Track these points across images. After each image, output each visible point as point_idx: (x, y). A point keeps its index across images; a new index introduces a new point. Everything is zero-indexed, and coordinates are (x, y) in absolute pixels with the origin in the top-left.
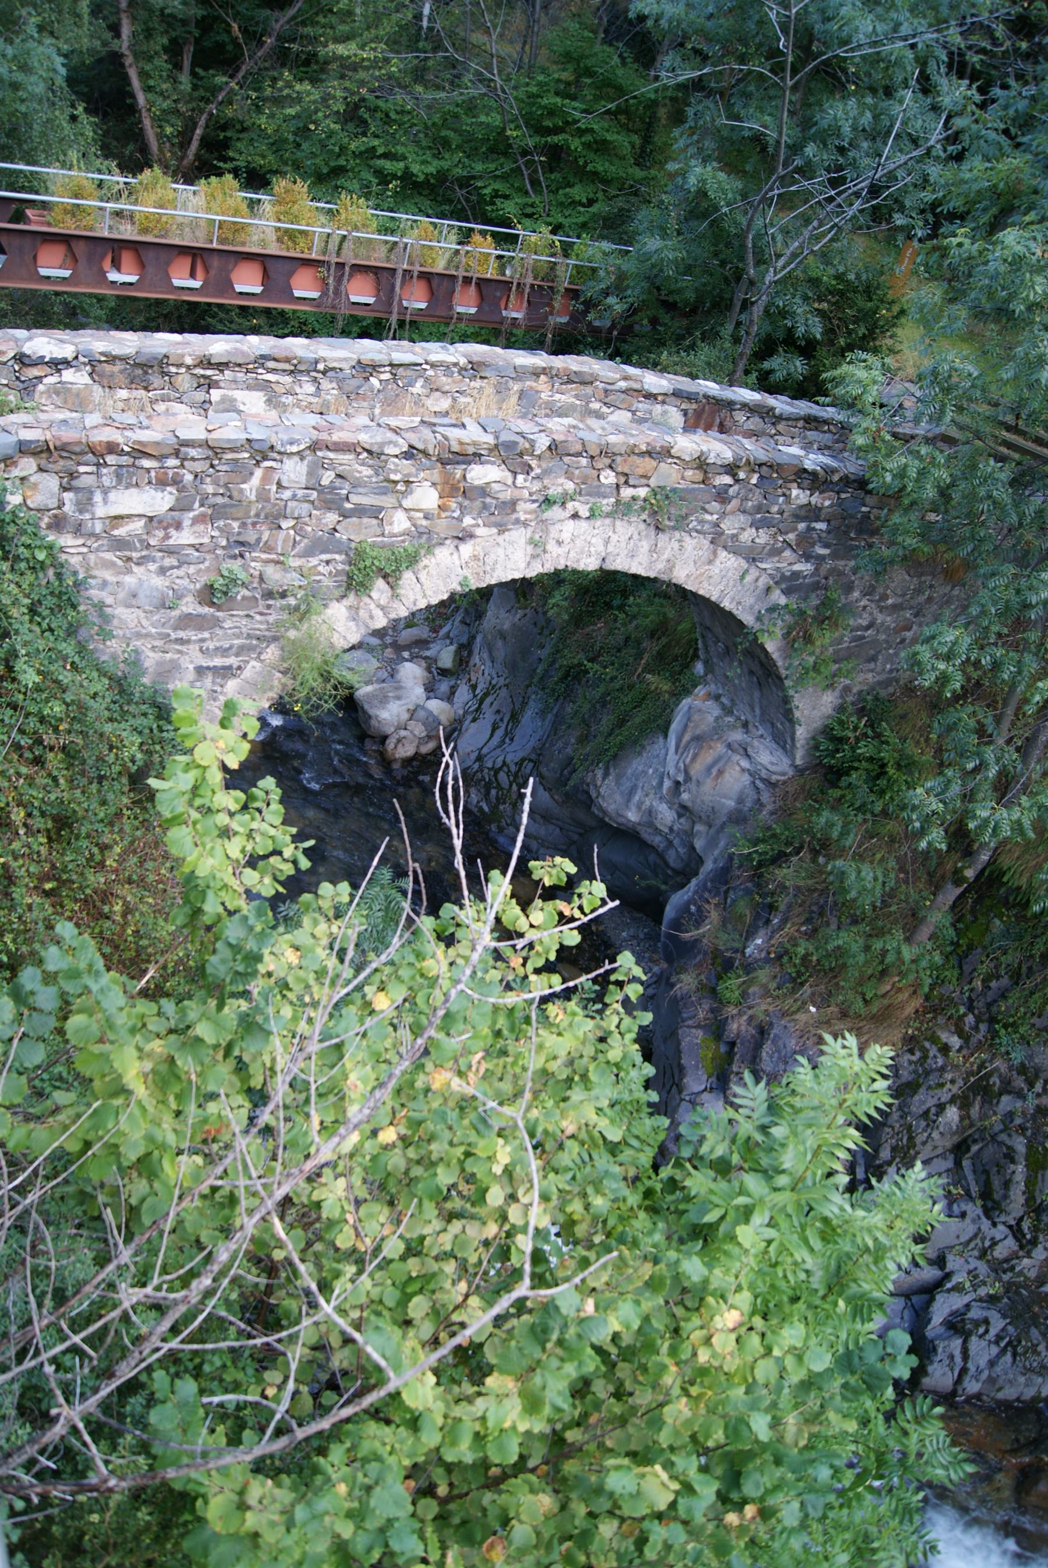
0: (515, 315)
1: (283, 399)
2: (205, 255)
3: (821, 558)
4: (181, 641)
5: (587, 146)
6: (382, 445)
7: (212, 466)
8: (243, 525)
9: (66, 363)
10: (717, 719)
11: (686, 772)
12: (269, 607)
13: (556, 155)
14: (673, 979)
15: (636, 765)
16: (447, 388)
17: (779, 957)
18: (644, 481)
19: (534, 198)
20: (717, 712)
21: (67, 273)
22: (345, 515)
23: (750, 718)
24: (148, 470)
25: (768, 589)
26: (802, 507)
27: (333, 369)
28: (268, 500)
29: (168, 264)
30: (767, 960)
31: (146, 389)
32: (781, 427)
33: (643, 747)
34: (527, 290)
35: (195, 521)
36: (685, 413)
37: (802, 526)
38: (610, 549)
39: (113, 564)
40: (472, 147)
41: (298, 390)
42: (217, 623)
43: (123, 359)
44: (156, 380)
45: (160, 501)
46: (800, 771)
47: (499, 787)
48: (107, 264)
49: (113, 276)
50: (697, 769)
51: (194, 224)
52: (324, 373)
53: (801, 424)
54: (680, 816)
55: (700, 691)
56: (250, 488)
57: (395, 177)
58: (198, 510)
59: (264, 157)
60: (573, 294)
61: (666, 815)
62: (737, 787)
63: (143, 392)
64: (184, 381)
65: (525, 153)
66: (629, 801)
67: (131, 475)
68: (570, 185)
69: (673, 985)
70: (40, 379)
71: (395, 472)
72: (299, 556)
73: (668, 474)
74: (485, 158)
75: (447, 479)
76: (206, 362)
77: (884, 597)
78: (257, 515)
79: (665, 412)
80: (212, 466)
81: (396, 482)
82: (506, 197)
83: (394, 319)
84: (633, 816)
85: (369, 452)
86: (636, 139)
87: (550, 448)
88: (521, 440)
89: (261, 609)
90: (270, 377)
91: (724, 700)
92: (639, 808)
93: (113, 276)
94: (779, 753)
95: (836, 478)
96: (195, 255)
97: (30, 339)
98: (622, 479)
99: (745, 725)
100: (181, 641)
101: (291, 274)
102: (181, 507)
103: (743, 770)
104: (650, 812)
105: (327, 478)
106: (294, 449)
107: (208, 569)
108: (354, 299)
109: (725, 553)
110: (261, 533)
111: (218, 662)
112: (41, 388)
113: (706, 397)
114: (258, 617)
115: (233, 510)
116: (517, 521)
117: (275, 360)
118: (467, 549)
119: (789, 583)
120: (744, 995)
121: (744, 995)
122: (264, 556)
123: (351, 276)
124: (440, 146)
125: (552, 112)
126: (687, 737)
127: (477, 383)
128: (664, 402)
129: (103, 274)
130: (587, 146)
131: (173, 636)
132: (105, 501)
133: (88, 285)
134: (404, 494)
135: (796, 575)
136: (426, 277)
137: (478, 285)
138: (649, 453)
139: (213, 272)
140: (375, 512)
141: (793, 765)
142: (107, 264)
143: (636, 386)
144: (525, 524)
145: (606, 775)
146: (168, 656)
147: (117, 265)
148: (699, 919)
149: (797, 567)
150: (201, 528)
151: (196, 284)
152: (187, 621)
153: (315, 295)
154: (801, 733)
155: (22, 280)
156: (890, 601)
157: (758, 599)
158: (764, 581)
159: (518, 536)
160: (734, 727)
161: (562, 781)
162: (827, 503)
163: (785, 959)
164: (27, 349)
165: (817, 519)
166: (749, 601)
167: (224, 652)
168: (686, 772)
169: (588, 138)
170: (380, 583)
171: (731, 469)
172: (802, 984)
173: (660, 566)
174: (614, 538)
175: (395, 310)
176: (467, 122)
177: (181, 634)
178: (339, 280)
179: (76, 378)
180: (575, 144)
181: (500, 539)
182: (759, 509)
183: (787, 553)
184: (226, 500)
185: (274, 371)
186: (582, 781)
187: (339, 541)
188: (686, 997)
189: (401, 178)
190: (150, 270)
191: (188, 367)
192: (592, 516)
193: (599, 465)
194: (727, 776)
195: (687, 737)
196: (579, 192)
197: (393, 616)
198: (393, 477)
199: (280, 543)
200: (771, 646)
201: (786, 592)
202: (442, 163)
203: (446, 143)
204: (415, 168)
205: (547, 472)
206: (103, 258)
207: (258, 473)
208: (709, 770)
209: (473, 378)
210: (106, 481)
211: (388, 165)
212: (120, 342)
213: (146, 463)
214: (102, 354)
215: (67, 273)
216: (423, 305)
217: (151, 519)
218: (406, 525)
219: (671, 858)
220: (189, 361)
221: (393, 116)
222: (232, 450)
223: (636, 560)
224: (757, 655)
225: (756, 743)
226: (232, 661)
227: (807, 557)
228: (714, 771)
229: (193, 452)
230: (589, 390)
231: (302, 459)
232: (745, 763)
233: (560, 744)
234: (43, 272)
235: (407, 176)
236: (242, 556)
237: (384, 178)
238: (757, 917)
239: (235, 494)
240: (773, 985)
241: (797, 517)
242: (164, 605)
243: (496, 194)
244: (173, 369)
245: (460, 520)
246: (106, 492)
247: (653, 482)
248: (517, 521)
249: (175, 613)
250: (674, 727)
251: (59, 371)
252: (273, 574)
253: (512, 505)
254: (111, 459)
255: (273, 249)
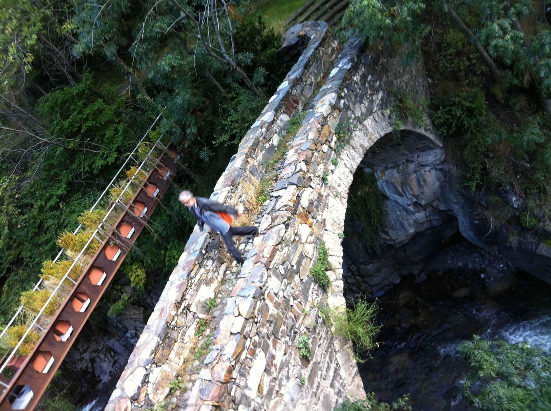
0: (168, 175)
1: (209, 277)
2: (78, 291)
3: (380, 85)
4: (318, 387)
5: (93, 119)
6: (279, 235)
7: (256, 323)
8: (284, 323)
9: (147, 376)
10: (398, 172)
11: (414, 196)
12: (319, 333)
13: (91, 133)
14: (508, 245)
15: (391, 218)
16: (236, 202)
17: (526, 193)
18: (331, 135)
19: (101, 152)
20: (395, 171)
21: (52, 360)
22: (297, 272)
23: (406, 158)
24: (247, 358)
25: (383, 114)
26: (361, 80)
27: (207, 246)
28: (280, 304)
29: (73, 309)
30: (524, 199)
31: (176, 341)
32: (304, 79)
33: (386, 211)
34: (161, 164)
35: (275, 347)
36: (284, 112)
37: (367, 85)
38: (348, 166)
39: (276, 403)
40: (63, 166)
41: (208, 268)
42: (317, 363)
43: (158, 345)
44: (174, 334)
45: (261, 360)
46: (445, 147)
47: (353, 285)
48: (58, 338)
49: (64, 338)
50: (416, 190)
51: (62, 289)
52: (207, 252)
53: (306, 71)
54: (425, 210)
55: (378, 175)
56: (273, 310)
57: (58, 203)
58: (270, 342)
59: (10, 255)
60: (172, 148)
61: (420, 216)
62: (434, 177)
63: (176, 344)
64: (181, 320)
65: (81, 145)
66: (405, 229)
67: (244, 368)
68: (104, 135)
69: (511, 247)
70: (147, 395)
71: (291, 237)
72: (305, 304)
73: (333, 123)
74: (72, 162)
75: (300, 215)
76: (178, 304)
77: (399, 72)
78: (283, 314)
79: (281, 121)
80: (256, 323)
81: (294, 240)
82: (93, 163)
83: (145, 223)
84: (412, 231)
85: (280, 243)
86: (100, 100)
87: (306, 164)
88: (299, 174)
89: (318, 338)
90: (198, 277)
91: (389, 166)
92: (410, 225)
93: (64, 338)
94: (431, 152)
95: (356, 59)
96: (77, 295)
97: (123, 390)
98: (328, 143)
99: (408, 161)
100: (318, 387)
101: (105, 257)
102: (265, 349)
103: (429, 171)
104: (415, 222)
105: (282, 270)
106: (265, 277)
107: (295, 354)
108: (129, 236)
109: (365, 122)
110: (291, 317)
111: (331, 373)
112: (151, 397)
113: (282, 100)
114: (321, 341)
115: (278, 324)
116: (326, 197)
117: (192, 271)
118: (328, 226)
119: (383, 105)
120: (535, 217)
121: (535, 217)
122: (300, 322)
123: (119, 232)
124: (55, 179)
125: (71, 125)
126: (400, 189)
127: (240, 187)
128: (277, 118)
129: (61, 342)
130: (93, 119)
131: (315, 390)
132: (250, 389)
133: (62, 353)
134: (300, 239)
135: (382, 99)
136: (136, 201)
137: (150, 183)
138: (323, 126)
139: (87, 292)
140: (302, 256)
141: (442, 148)
142: (58, 338)
143: (267, 125)
144: (329, 195)
145: (387, 233)
146: (321, 399)
147: (60, 334)
148: (485, 221)
149: (380, 98)
150: (278, 345)
151: (88, 301)
152: (311, 378)
153: (119, 252)
154: (432, 137)
155: (43, 383)
156: (401, 71)
157: (385, 120)
158: (379, 113)
159: (331, 201)
160: (407, 166)
161: (375, 255)
162: (363, 69)
163: (528, 191)
164: (131, 391)
165: (367, 77)
166: (384, 124)
167: (328, 368)
168: (414, 196)
169: (90, 118)
170: (328, 273)
171: (340, 97)
172: (545, 189)
173: (361, 150)
174: (345, 162)
175: (143, 221)
176: (55, 162)
177: (315, 385)
178: (119, 238)
179: (156, 374)
180: (89, 123)
181: (330, 209)
182: (356, 97)
183: (374, 97)
184: (272, 325)
185: (196, 274)
186: (381, 245)
187: (307, 281)
188: (520, 244)
189: (61, 200)
190: (71, 320)
191: (176, 315)
192: (335, 164)
193: (319, 148)
194: (428, 179)
195: (400, 189)
196: (109, 133)
197: (341, 276)
198: (292, 239)
199: (298, 310)
200: (402, 128)
201: (387, 107)
202: (64, 181)
203: (56, 175)
204: (60, 192)
205: (314, 172)
206: (54, 339)
207: (268, 301)
208: (419, 185)
209: (237, 188)
210: (242, 384)
211: (52, 203)
212: (146, 343)
213: (243, 357)
214: (151, 355)
215: (52, 360)
216: (146, 209)
217: (265, 370)
218: (312, 246)
219: (435, 223)
220: (174, 313)
221: (32, 190)
222: (254, 309)
223: (356, 159)
224: (405, 134)
225: (420, 160)
226: (333, 366)
227: (377, 91)
228: (422, 183)
229: (248, 329)
230: (261, 144)
231: (270, 276)
232: (427, 169)
233: (355, 248)
234: (45, 371)
235: (61, 198)
236: (296, 333)
237: (56, 208)
238: (500, 195)
239: (271, 319)
240: (538, 202)
241: (364, 84)
242: (301, 385)
243: (90, 166)
244: (173, 323)
245: (317, 221)
246: (246, 387)
247: (333, 131)
248: (326, 197)
249: (306, 381)
250: (388, 193)
251: (148, 382)
252: (309, 321)
253: (320, 195)
254: (235, 374)
255: (91, 261)
